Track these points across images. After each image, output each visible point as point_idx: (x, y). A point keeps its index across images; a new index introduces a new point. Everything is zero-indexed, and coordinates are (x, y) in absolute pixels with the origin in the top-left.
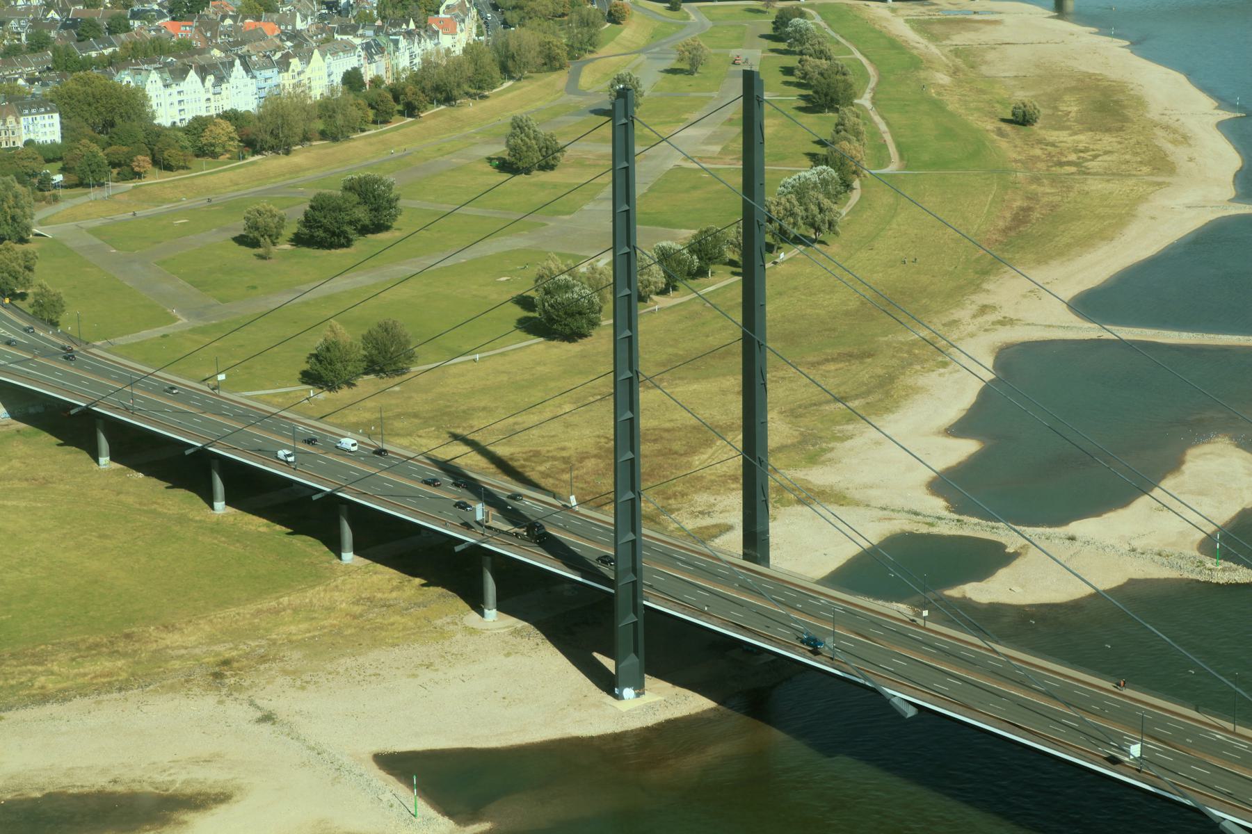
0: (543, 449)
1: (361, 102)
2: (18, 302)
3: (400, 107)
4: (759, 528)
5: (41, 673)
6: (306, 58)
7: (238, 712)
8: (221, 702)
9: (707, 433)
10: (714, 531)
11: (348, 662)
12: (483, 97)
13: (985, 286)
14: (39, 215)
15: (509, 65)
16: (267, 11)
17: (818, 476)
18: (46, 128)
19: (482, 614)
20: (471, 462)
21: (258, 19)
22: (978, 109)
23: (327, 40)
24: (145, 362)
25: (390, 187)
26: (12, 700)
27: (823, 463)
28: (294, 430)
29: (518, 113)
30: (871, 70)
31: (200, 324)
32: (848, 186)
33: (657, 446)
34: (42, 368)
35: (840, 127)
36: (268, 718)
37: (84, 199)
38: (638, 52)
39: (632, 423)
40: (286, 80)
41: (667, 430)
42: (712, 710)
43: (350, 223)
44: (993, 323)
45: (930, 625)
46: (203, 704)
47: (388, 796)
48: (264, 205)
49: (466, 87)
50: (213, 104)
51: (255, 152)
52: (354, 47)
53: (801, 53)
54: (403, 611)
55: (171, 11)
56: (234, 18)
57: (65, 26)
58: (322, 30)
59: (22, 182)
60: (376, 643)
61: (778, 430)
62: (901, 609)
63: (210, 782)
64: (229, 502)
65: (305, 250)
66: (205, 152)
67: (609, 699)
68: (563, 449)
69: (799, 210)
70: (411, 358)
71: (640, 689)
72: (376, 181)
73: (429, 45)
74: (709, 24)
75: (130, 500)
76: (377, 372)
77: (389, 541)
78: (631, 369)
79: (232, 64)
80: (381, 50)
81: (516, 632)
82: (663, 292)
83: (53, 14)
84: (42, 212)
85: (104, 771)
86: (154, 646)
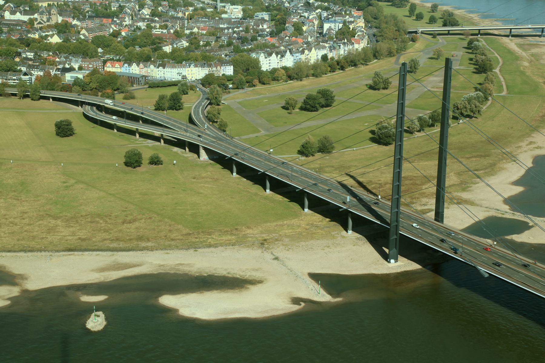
0: (373, 180)
1: (326, 65)
2: (215, 124)
3: (339, 67)
4: (440, 211)
5: (210, 238)
6: (310, 50)
7: (268, 256)
8: (262, 252)
9: (427, 179)
10: (427, 211)
11: (303, 243)
12: (367, 65)
13: (533, 135)
14: (224, 97)
15: (376, 55)
16: (300, 35)
17: (465, 195)
18: (229, 70)
19: (347, 232)
20: (350, 182)
21: (297, 37)
22: (537, 75)
23: (317, 45)
24: (249, 144)
25: (332, 93)
26: (201, 245)
27: (468, 191)
28: (292, 168)
29: (377, 70)
30: (500, 60)
31: (268, 133)
32: (487, 99)
33: (411, 182)
34: (218, 144)
35: (486, 79)
36: (276, 258)
37: (238, 93)
38: (420, 52)
39: (399, 173)
40: (303, 57)
41: (415, 177)
42: (420, 269)
43: (318, 104)
44: (534, 148)
45: (496, 247)
46: (257, 252)
47: (311, 287)
48: (292, 96)
49: (361, 61)
50: (279, 64)
51: (291, 80)
52: (326, 47)
53: (476, 53)
54: (322, 229)
55: (270, 35)
56: (289, 37)
57: (238, 39)
58: (316, 41)
59: (219, 87)
60: (312, 238)
61: (451, 179)
62: (489, 241)
63: (257, 276)
64: (271, 190)
65: (303, 112)
66: (275, 79)
67: (386, 262)
68: (380, 180)
69: (468, 106)
70: (333, 148)
71: (396, 260)
72: (328, 91)
73: (351, 47)
74: (445, 43)
75: (241, 187)
76: (322, 152)
77: (320, 206)
78: (400, 155)
79: (286, 52)
80: (334, 48)
81: (358, 239)
82: (419, 131)
83: (235, 35)
84: (225, 96)
85: (226, 270)
86: (244, 233)
